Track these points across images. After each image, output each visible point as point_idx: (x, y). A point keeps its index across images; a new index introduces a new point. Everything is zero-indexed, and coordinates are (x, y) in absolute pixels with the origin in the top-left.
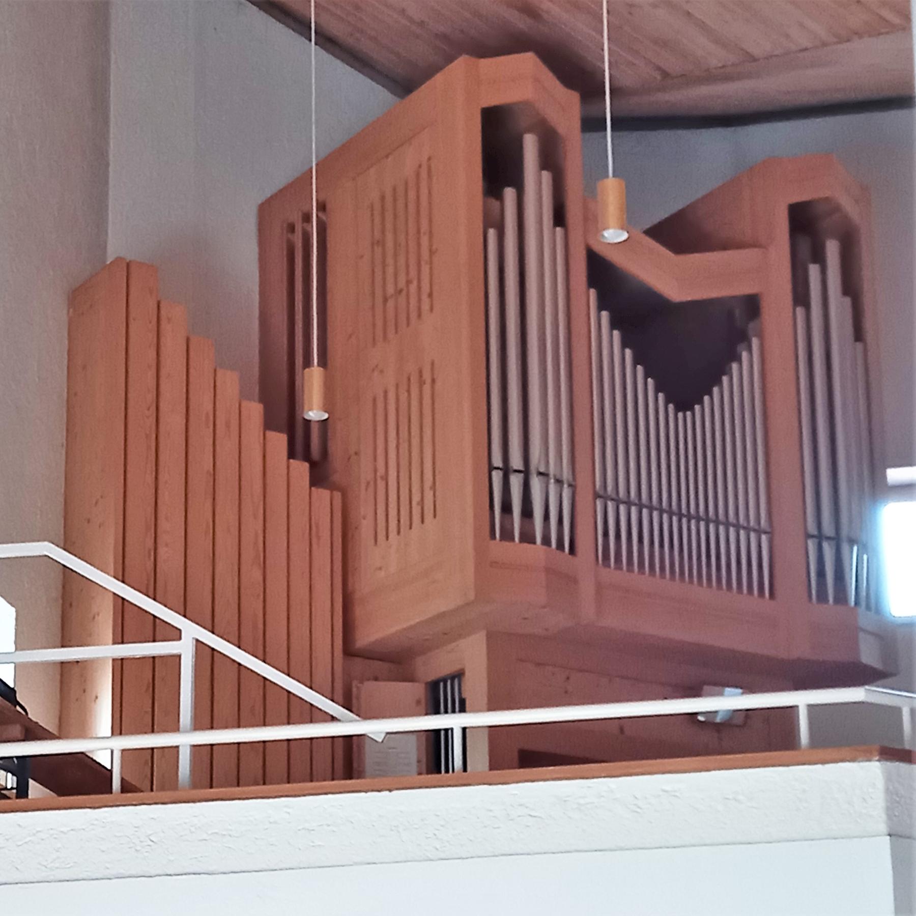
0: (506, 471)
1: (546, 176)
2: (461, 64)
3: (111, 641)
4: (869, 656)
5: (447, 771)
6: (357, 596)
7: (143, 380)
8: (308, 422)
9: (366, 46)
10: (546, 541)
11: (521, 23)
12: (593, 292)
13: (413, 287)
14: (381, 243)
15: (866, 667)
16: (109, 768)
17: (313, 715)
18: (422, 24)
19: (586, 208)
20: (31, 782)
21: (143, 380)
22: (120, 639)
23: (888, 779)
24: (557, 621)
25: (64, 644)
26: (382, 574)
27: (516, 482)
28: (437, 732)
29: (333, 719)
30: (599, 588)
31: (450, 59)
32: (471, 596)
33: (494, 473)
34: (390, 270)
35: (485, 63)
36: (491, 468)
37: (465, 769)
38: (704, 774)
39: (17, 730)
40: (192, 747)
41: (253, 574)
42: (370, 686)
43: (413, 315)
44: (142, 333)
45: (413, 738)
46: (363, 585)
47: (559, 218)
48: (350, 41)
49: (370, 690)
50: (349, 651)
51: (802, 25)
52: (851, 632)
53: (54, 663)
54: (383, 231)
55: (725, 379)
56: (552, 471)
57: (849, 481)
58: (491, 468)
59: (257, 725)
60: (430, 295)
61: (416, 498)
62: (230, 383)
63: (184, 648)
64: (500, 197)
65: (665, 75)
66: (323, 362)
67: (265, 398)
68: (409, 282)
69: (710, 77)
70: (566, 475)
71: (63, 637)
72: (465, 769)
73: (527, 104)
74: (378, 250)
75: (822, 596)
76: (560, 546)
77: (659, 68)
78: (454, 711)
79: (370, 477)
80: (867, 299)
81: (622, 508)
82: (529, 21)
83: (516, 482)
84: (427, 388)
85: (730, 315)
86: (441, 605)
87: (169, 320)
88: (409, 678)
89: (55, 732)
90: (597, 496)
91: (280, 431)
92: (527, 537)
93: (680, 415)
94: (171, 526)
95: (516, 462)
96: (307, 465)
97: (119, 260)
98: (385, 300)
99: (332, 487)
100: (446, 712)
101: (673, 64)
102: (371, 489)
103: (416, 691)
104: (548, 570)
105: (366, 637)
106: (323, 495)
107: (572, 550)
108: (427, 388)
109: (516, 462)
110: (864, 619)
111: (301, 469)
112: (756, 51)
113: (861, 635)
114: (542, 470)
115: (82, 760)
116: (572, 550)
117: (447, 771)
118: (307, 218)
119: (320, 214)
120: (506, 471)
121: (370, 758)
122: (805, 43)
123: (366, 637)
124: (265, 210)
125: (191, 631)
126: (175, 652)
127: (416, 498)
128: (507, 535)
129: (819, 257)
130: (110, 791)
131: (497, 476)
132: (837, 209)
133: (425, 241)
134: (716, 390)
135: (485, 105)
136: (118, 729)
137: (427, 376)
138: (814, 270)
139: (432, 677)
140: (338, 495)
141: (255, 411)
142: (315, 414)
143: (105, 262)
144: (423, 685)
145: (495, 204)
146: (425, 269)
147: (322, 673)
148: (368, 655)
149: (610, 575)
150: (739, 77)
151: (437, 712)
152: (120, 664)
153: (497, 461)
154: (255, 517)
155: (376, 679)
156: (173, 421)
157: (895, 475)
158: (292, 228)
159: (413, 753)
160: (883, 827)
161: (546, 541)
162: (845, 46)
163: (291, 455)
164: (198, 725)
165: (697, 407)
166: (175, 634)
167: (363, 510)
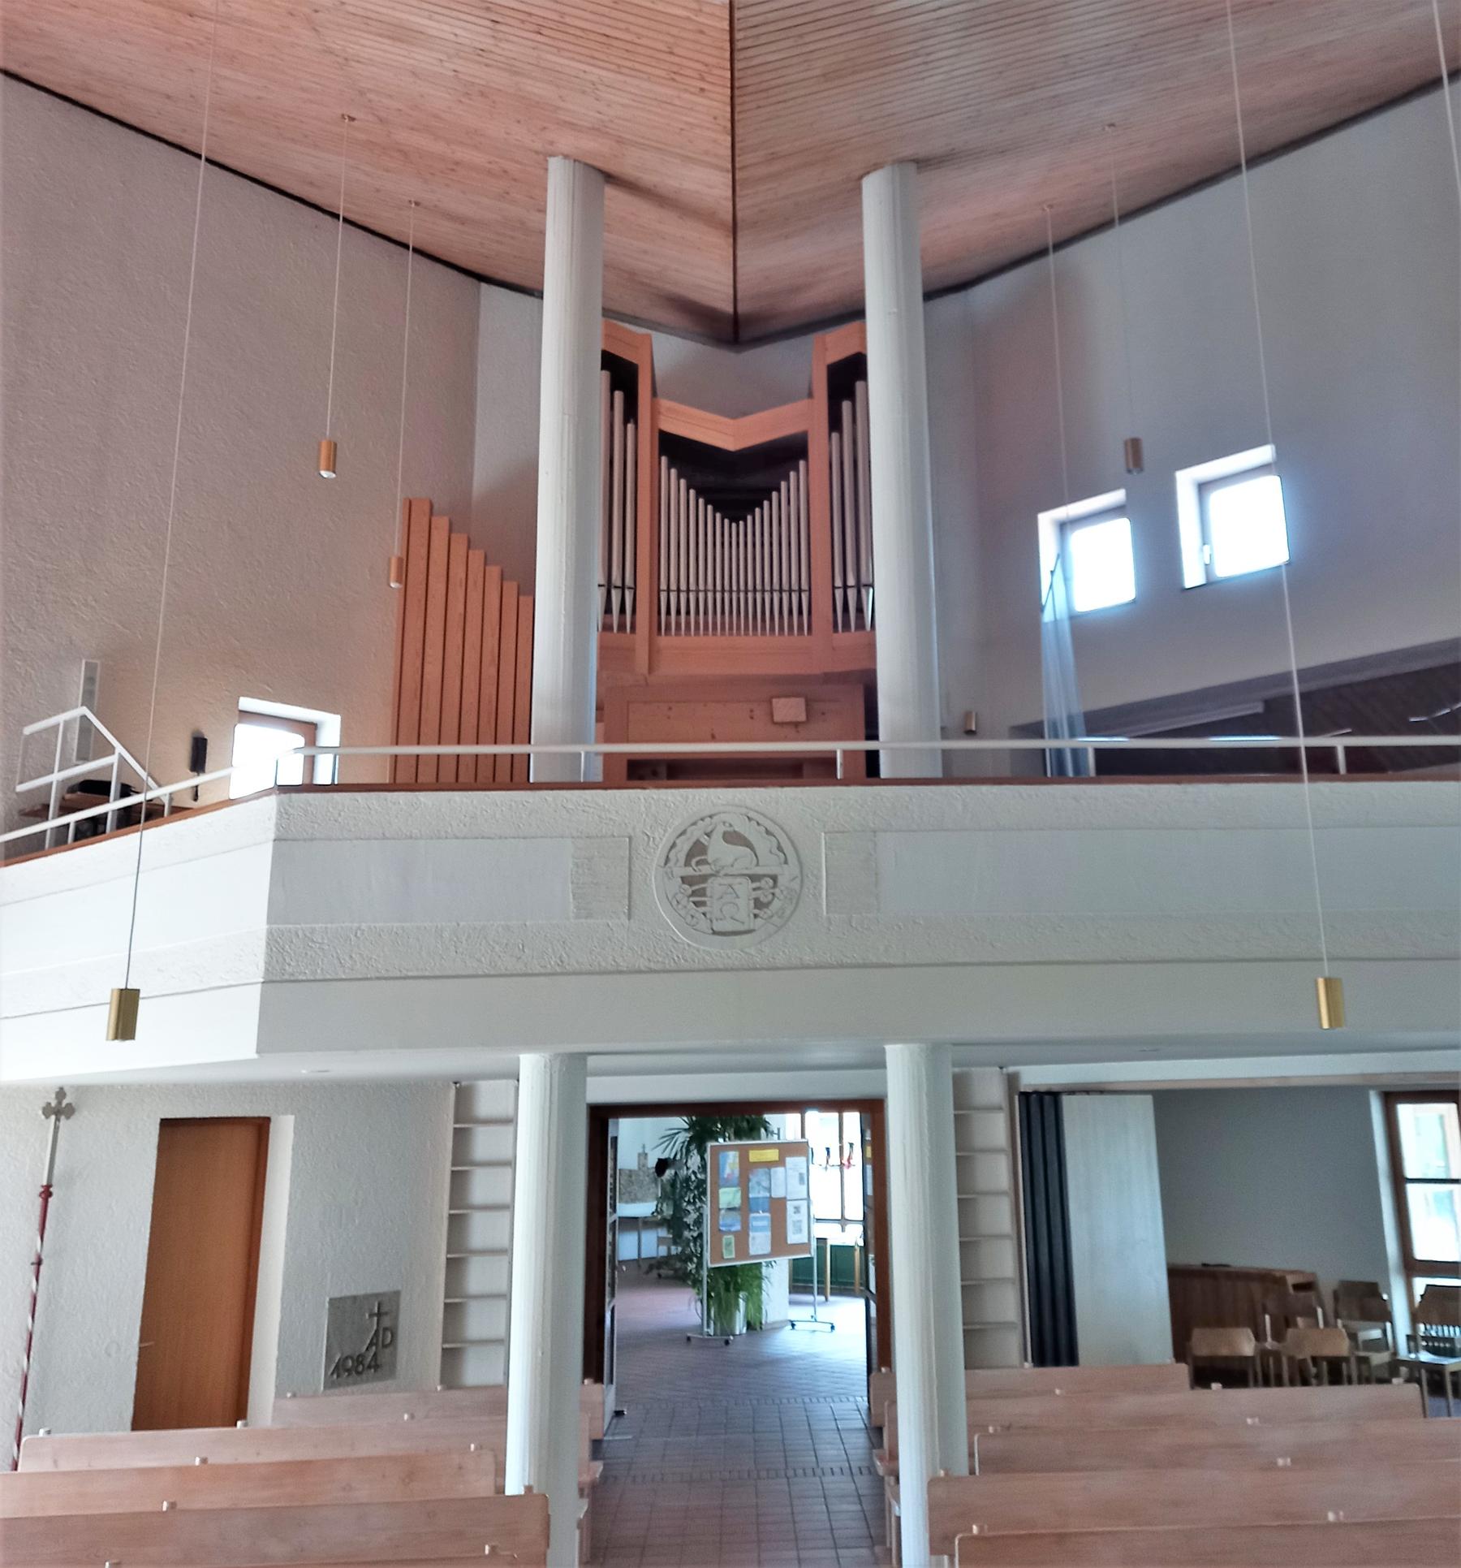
93: (734, 525)
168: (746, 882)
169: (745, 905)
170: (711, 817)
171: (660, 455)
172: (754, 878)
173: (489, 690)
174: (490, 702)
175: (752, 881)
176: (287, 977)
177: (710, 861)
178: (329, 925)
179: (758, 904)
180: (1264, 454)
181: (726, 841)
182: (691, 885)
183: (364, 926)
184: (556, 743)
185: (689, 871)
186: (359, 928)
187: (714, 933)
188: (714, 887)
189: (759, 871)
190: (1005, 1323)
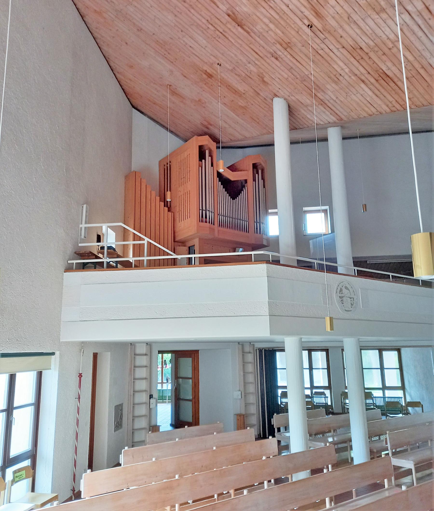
0: (202, 210)
1: (210, 158)
2: (195, 137)
3: (132, 240)
4: (265, 243)
5: (192, 264)
6: (176, 231)
7: (138, 192)
8: (167, 202)
9: (178, 133)
10: (209, 222)
11: (206, 130)
12: (218, 178)
13: (186, 177)
14: (181, 169)
15: (264, 245)
16: (108, 228)
17: (168, 254)
18: (188, 129)
19: (217, 164)
20: (118, 264)
21: (138, 192)
22: (134, 240)
23: (267, 267)
24: (211, 237)
25: (124, 241)
26: (180, 228)
27: (204, 212)
28: (190, 258)
29: (172, 255)
30: (218, 231)
31: (194, 136)
32: (196, 232)
33: (200, 210)
34: (182, 174)
35: (199, 137)
36: (200, 210)
37: (195, 264)
38: (236, 266)
39: (116, 256)
40: (236, 416)
41: (158, 227)
42: (178, 247)
43: (186, 182)
44: (138, 184)
45: (186, 259)
46: (177, 229)
47: (212, 165)
48: (175, 132)
49: (178, 248)
50: (174, 241)
51: (255, 132)
52: (262, 239)
53: (122, 244)
54: (181, 167)
55: (241, 194)
56: (211, 210)
57: (262, 210)
58: (200, 210)
59: (158, 256)
60: (189, 178)
61: (186, 214)
62: (153, 193)
63: (145, 242)
64: (202, 161)
65: (231, 140)
66: (170, 191)
67: (160, 196)
68: (185, 176)
69: (239, 140)
70: (213, 211)
71: (124, 240)
72: (195, 264)
73: (207, 145)
74: (180, 170)
75: (257, 233)
76: (212, 223)
77: (230, 139)
78: (193, 254)
79: (178, 210)
80: (266, 180)
81: (223, 217)
82: (207, 130)
83: (204, 212)
84: (188, 195)
85: (242, 183)
86: (191, 234)
87: (143, 182)
88: (185, 246)
89: (122, 256)
90: (218, 215)
91: (163, 202)
92: (206, 222)
93: (233, 200)
94: (143, 219)
95: (204, 208)
96: (167, 208)
97: (134, 171)
98: (181, 179)
99: (172, 212)
100: (191, 254)
101: (232, 138)
102: (178, 213)
103: (186, 249)
104: (210, 228)
105: (177, 239)
106: (170, 213)
107: (214, 224)
108: (188, 195)
109: (204, 208)
110: (264, 237)
111: (166, 209)
112: (247, 136)
113: (264, 239)
114: (209, 210)
115: (128, 261)
116: (214, 224)
117: (192, 264)
118: (167, 164)
119: (170, 163)
120: (202, 210)
121: (178, 262)
122: (256, 135)
123: (177, 239)
124: (160, 162)
125: (147, 239)
126: (144, 243)
127: (186, 214)
128: (202, 221)
129: (258, 173)
130: (132, 267)
131: (201, 211)
132: (261, 164)
133: (188, 169)
134: (239, 196)
135: (200, 145)
136: (134, 256)
137: (188, 193)
138: (257, 175)
139: (189, 246)
140: (173, 214)
141: (158, 198)
142: (169, 200)
143: (131, 171)
144: (187, 247)
145: (201, 162)
146: (188, 174)
147: (170, 246)
148: (177, 242)
149: (220, 228)
150: (245, 140)
151: (190, 254)
152: (134, 245)
153: (201, 208)
154: (158, 217)
155: (179, 246)
156: (143, 200)
157: (270, 211)
158: (165, 166)
159: (186, 261)
160: (266, 276)
161: (209, 222)
162: (263, 136)
163: (164, 206)
164: (147, 256)
165: (236, 199)
166: (144, 240)
167: (177, 215)
168: (349, 298)
169: (350, 305)
170: (342, 282)
171: (217, 177)
172: (351, 298)
173: (157, 232)
174: (158, 235)
175: (350, 299)
176: (273, 314)
177: (343, 293)
178: (280, 301)
179: (352, 305)
180: (304, 208)
181: (345, 288)
182: (341, 298)
183: (286, 302)
184: (292, 256)
185: (340, 295)
186: (285, 303)
187: (346, 311)
188: (344, 299)
189: (351, 296)
190: (250, 403)
